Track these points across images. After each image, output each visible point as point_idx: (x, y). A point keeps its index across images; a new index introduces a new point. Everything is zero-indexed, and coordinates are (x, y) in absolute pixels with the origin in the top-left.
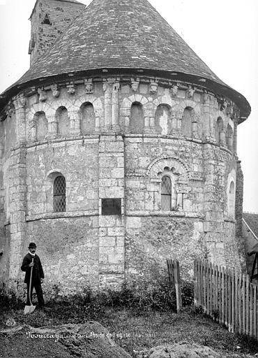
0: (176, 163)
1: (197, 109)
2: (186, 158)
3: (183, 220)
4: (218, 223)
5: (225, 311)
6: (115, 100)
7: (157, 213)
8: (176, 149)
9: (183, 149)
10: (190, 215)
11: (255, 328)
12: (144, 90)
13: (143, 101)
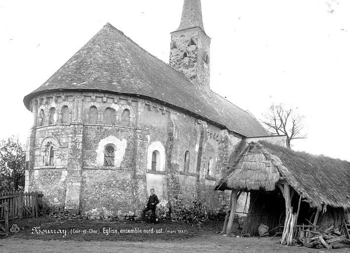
0: (52, 139)
1: (70, 105)
2: (58, 135)
3: (55, 170)
4: (75, 171)
5: (27, 201)
6: (80, 104)
7: (44, 167)
8: (53, 131)
9: (57, 131)
10: (58, 167)
11: (286, 220)
12: (99, 100)
13: (97, 105)
